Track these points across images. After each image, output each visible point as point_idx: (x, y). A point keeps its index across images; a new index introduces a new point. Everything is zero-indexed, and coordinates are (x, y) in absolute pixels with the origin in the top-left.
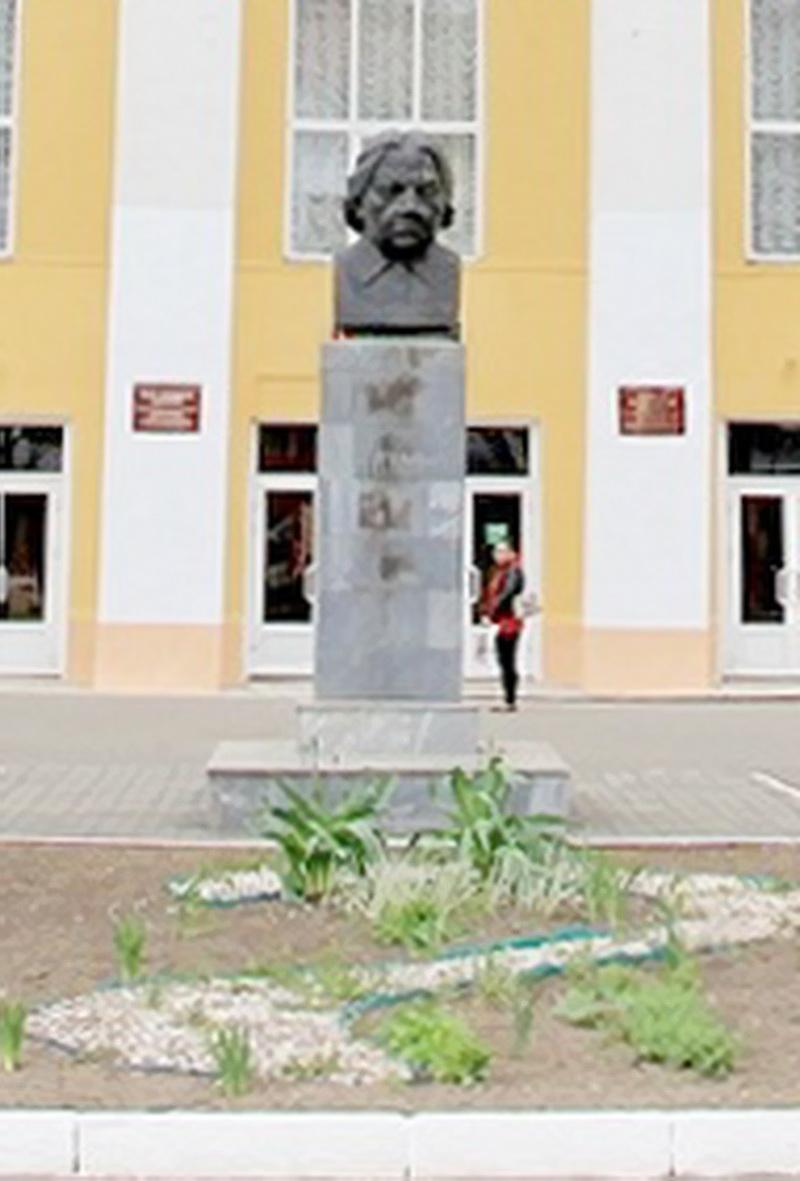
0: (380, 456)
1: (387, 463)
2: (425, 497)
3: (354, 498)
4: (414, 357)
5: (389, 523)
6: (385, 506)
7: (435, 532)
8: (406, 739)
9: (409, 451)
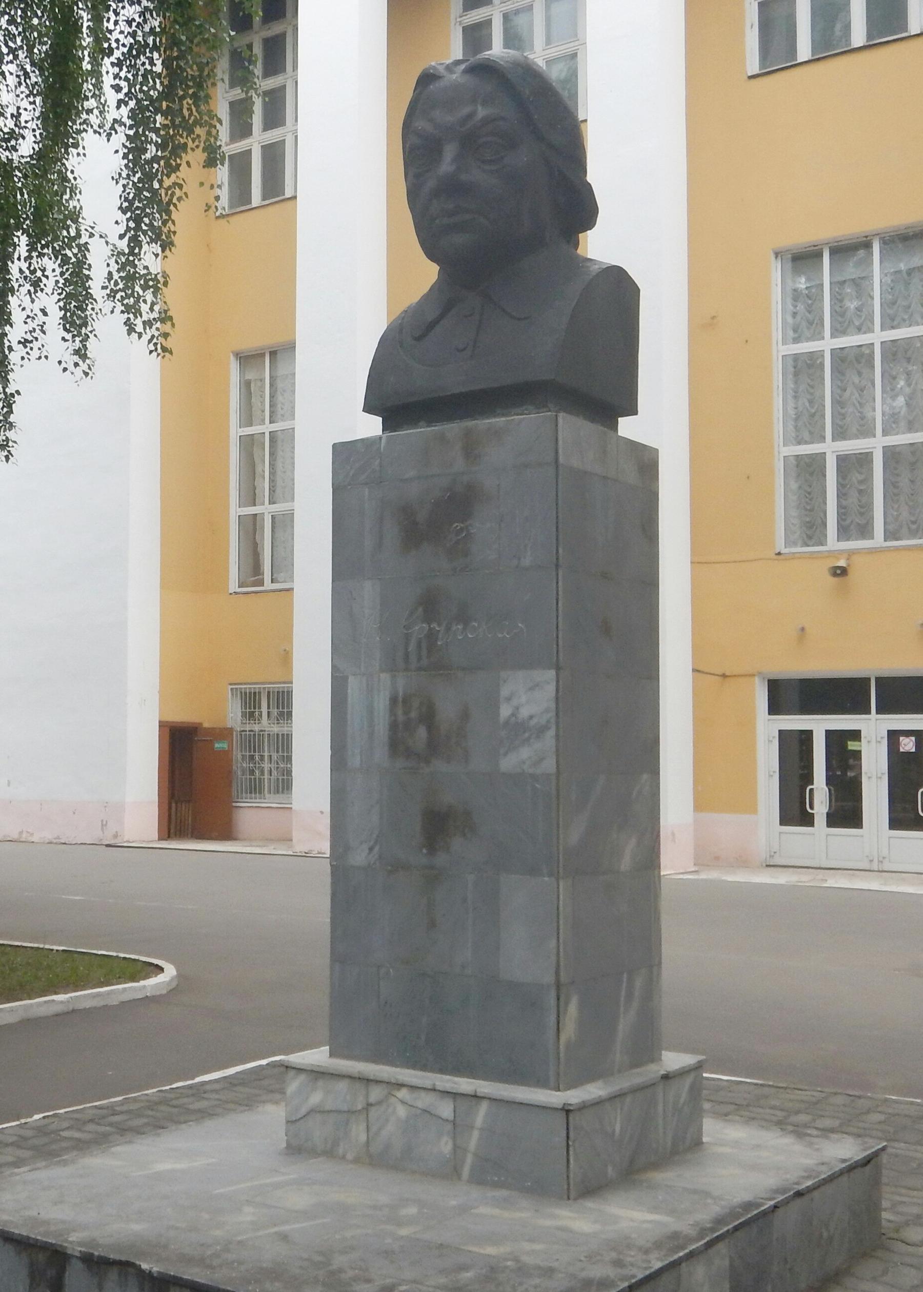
0: (419, 629)
1: (431, 636)
2: (492, 702)
3: (381, 703)
4: (471, 449)
5: (434, 747)
6: (429, 717)
7: (508, 763)
8: (445, 1146)
9: (464, 617)
